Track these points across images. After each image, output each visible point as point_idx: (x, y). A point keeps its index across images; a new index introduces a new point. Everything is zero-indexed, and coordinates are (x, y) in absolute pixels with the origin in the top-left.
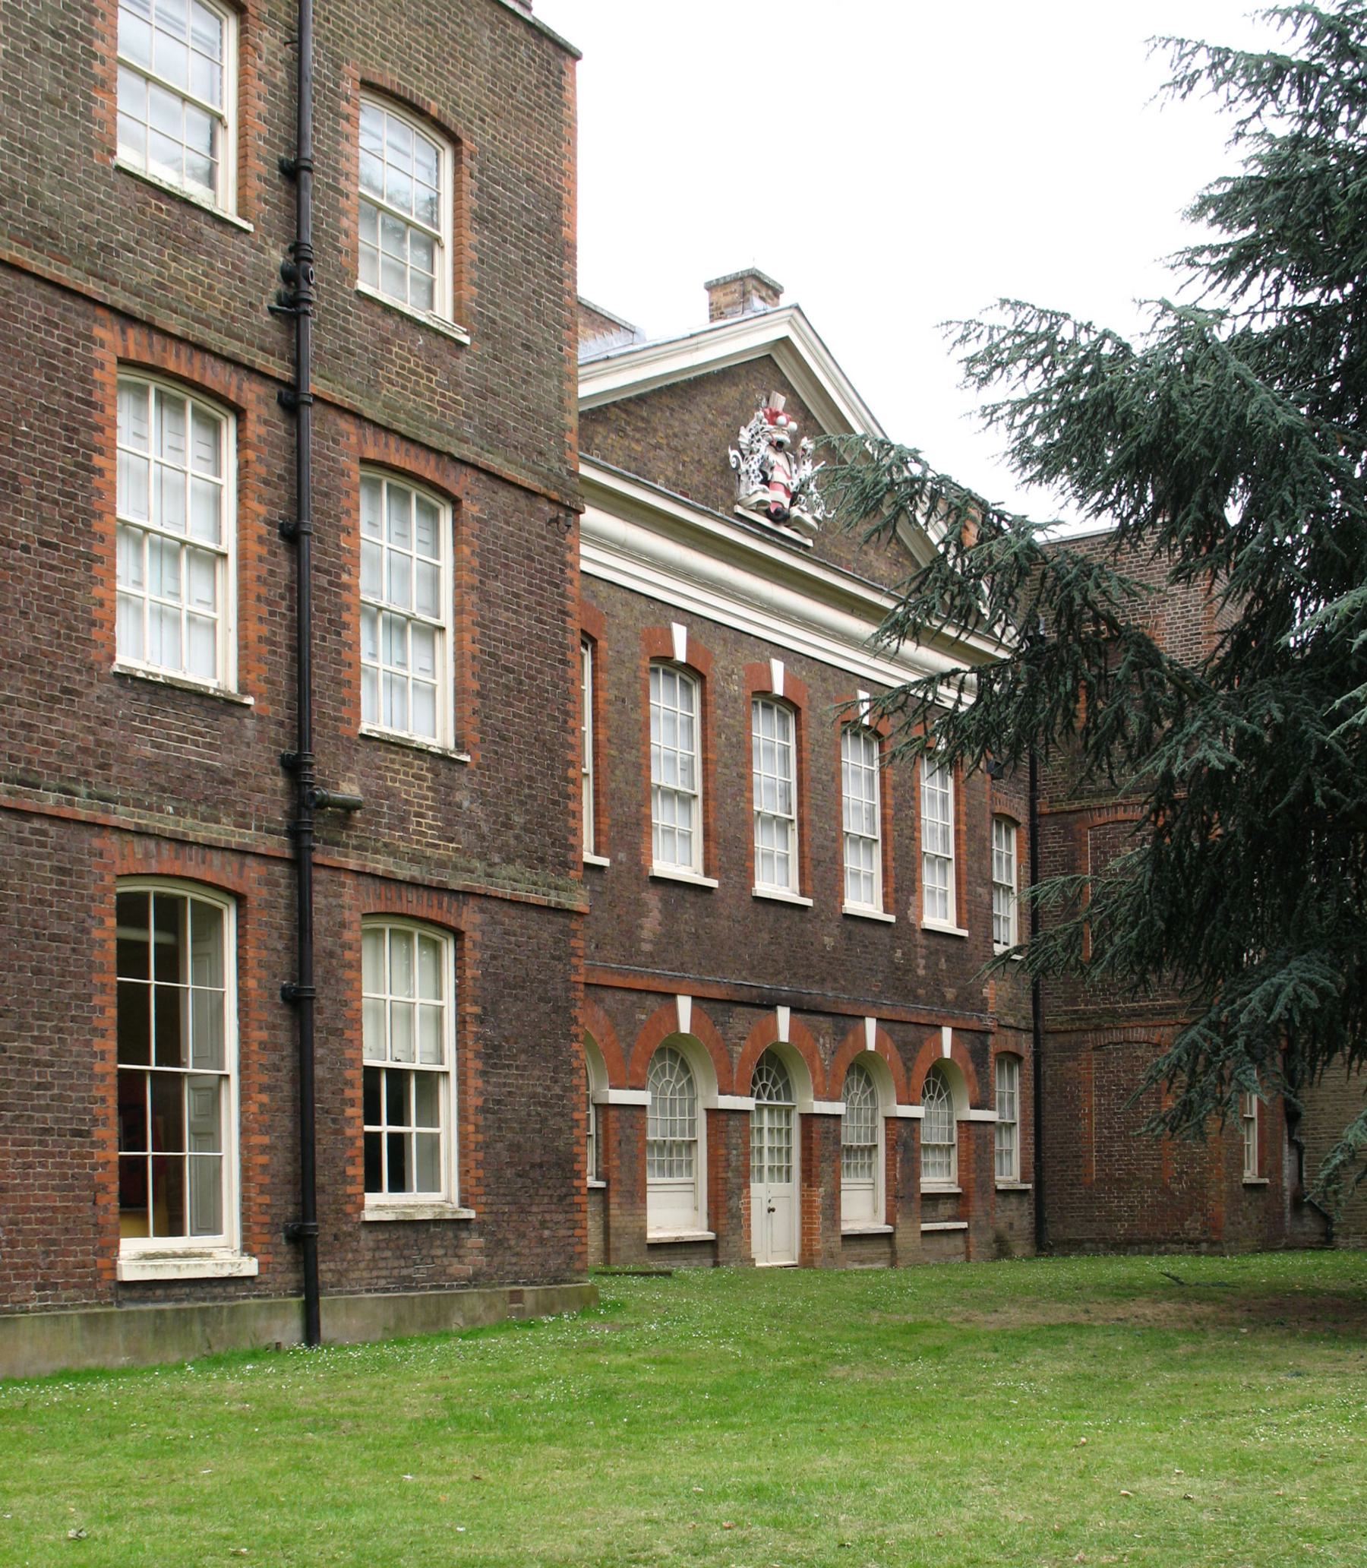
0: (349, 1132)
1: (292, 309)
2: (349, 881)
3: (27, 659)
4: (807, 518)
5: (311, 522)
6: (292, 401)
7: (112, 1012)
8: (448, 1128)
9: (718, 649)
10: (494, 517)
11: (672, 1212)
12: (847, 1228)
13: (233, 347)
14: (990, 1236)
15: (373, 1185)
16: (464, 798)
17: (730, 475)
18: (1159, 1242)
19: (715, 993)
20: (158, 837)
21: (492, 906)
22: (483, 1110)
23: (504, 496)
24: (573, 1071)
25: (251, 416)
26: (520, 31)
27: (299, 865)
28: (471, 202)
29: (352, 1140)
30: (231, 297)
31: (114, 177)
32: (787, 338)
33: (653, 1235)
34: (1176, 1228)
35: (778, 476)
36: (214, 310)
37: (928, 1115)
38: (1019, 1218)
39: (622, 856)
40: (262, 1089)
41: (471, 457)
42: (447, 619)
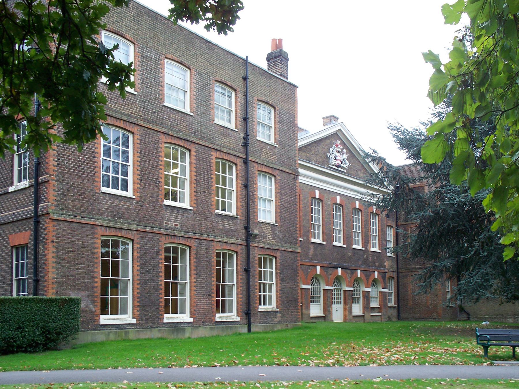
0: (256, 294)
1: (246, 144)
2: (256, 248)
3: (201, 212)
4: (345, 166)
5: (250, 183)
6: (246, 162)
7: (215, 274)
8: (274, 294)
9: (325, 195)
10: (282, 178)
11: (316, 310)
12: (354, 314)
13: (235, 153)
14: (387, 317)
15: (260, 305)
16: (277, 232)
17: (328, 159)
18: (426, 318)
19: (325, 265)
20: (223, 242)
21: (282, 252)
22: (281, 290)
23: (284, 174)
24: (298, 283)
25: (238, 165)
26: (286, 84)
27: (247, 246)
28: (278, 119)
29: (257, 296)
30: (234, 144)
31: (214, 125)
32: (340, 130)
33: (312, 315)
34: (430, 315)
35: (338, 158)
36: (232, 146)
37: (372, 291)
38: (394, 313)
39: (305, 238)
40: (241, 287)
41: (278, 168)
42: (273, 198)
